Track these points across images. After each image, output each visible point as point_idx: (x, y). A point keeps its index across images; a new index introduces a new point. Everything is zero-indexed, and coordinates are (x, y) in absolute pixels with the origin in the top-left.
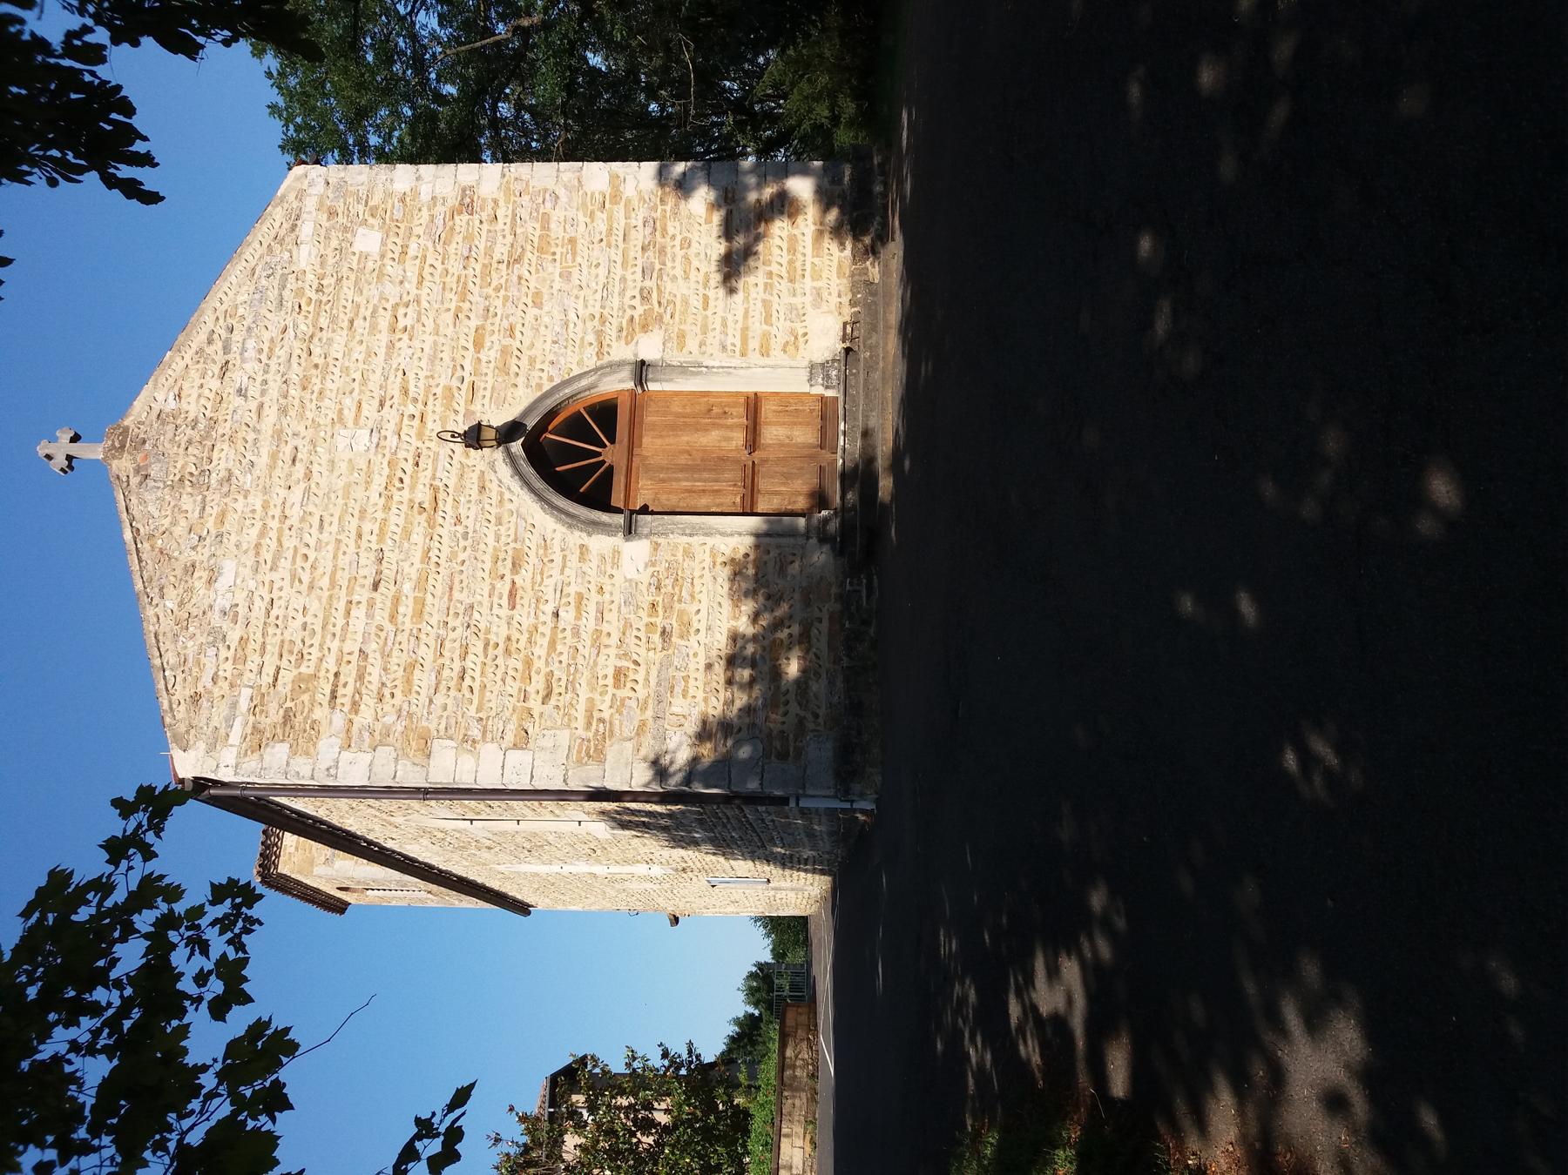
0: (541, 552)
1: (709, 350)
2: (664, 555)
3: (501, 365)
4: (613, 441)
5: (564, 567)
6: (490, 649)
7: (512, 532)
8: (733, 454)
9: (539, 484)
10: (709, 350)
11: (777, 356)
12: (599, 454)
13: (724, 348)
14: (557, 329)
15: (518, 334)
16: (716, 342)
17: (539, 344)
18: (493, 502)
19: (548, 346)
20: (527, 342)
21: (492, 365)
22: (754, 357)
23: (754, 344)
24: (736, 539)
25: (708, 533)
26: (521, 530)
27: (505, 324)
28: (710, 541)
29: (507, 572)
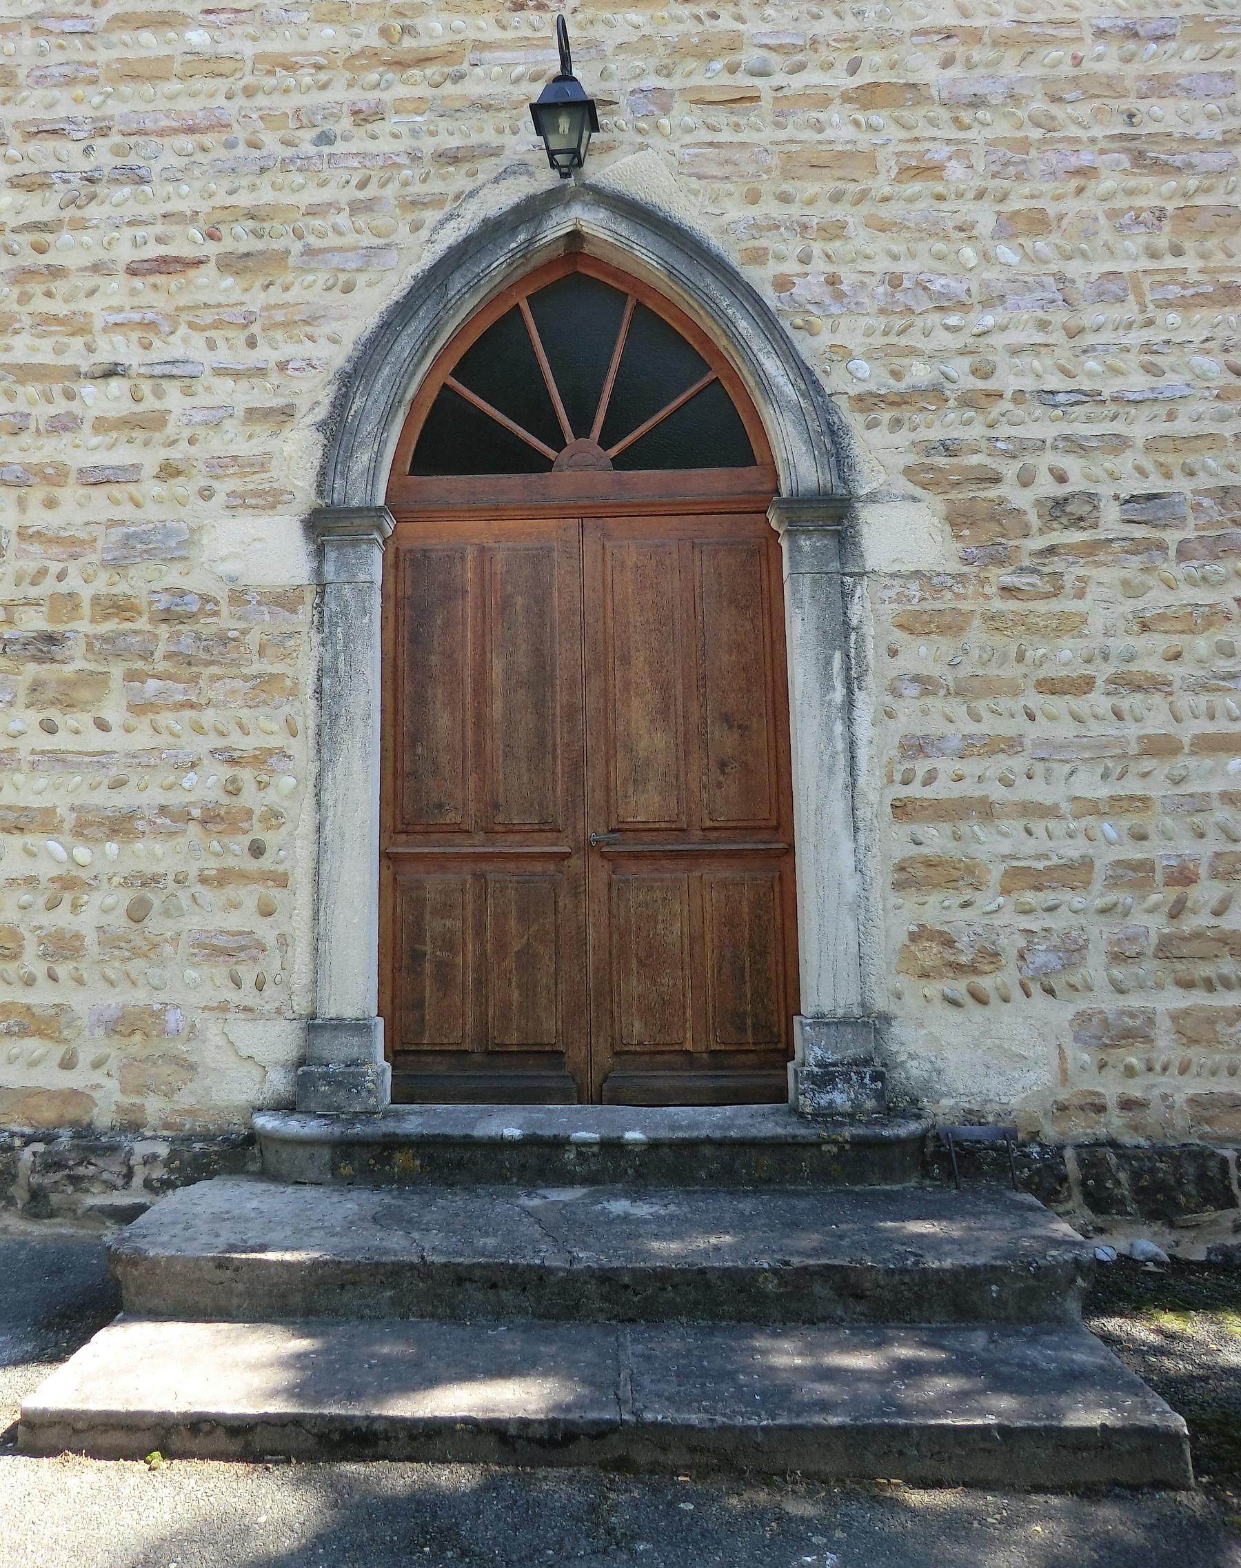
0: (279, 316)
2: (264, 624)
4: (619, 463)
6: (250, 224)
7: (333, 240)
16: (935, 726)
19: (882, 265)
23: (935, 839)
25: (325, 740)
26: (336, 260)
27: (940, 152)
28: (302, 749)
29: (227, 245)
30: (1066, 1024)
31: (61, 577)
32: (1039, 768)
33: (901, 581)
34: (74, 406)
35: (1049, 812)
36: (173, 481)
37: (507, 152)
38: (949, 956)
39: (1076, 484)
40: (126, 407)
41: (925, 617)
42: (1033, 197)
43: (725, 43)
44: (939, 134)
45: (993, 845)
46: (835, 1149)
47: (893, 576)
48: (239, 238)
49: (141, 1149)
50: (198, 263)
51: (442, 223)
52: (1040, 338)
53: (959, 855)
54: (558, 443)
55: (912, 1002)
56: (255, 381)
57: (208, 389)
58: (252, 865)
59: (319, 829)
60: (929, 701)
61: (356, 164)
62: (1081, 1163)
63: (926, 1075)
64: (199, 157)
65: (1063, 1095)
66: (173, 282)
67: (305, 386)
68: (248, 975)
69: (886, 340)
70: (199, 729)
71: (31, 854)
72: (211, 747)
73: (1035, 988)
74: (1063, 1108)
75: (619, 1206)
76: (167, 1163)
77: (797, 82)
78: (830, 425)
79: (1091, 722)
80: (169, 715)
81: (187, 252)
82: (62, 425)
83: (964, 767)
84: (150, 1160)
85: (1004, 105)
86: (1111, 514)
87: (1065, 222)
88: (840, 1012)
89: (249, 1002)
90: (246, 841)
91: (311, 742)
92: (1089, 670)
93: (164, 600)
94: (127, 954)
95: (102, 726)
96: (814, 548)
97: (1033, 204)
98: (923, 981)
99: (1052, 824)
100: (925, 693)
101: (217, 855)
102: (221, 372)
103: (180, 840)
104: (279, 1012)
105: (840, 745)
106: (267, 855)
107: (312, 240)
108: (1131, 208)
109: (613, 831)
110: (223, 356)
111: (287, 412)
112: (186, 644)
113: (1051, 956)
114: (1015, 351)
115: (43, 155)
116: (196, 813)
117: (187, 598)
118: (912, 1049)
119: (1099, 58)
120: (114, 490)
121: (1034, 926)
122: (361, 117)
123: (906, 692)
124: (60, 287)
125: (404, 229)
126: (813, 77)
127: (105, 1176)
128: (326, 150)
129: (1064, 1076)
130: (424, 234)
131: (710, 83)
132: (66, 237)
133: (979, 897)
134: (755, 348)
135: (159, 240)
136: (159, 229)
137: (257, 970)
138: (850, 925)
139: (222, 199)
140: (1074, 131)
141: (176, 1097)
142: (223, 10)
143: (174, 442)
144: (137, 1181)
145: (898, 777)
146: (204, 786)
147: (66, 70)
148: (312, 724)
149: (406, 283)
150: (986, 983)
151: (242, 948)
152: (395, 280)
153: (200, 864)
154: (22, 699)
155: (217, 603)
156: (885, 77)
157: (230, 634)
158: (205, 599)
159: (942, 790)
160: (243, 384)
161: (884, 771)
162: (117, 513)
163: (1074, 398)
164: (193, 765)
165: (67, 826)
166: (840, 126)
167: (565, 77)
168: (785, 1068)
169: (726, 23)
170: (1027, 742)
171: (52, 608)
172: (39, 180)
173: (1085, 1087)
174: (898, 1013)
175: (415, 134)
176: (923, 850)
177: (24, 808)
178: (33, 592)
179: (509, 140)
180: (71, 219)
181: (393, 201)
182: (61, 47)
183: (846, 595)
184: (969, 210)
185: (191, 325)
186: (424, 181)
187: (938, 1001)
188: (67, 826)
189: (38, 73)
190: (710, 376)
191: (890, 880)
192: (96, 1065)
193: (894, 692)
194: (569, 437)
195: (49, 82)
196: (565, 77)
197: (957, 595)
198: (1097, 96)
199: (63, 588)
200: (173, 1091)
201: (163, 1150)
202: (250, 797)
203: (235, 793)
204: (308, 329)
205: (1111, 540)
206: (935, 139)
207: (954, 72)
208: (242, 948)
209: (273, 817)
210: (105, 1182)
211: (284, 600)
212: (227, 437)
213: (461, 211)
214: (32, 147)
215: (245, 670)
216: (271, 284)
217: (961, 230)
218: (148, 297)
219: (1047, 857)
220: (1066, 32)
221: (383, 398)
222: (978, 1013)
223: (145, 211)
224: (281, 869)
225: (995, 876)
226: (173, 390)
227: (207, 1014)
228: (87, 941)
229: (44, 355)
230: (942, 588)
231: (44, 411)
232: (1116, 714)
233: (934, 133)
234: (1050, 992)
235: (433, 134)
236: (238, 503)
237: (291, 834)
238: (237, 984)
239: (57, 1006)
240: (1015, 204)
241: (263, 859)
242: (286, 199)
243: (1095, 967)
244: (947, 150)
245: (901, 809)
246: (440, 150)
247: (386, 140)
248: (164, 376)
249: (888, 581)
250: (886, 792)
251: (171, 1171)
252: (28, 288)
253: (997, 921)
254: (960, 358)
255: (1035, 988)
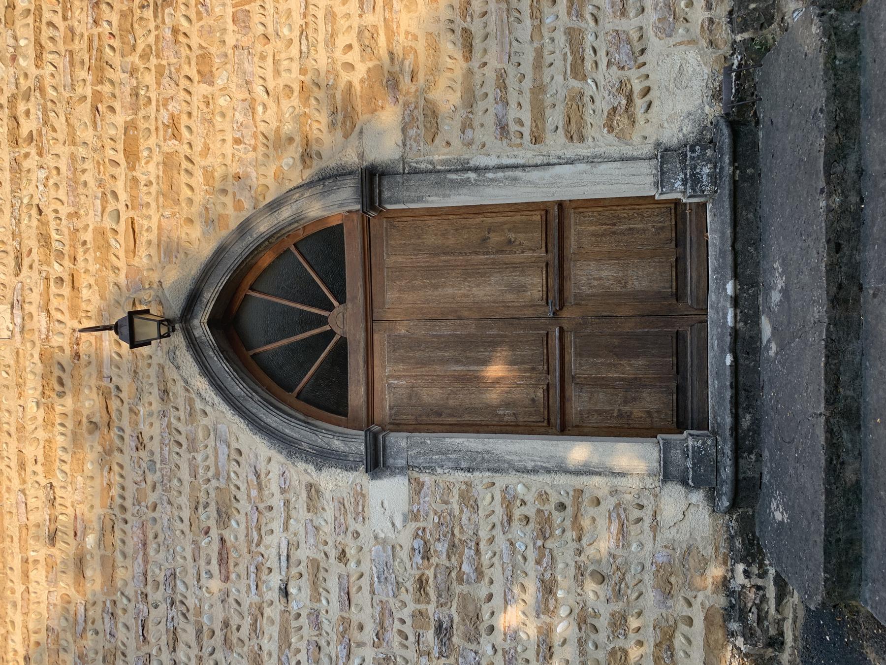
2: (429, 501)
4: (342, 300)
7: (211, 461)
16: (490, 120)
19: (228, 149)
23: (555, 117)
25: (498, 467)
26: (222, 458)
27: (165, 116)
28: (501, 480)
29: (212, 523)
30: (662, 42)
31: (403, 622)
32: (514, 59)
34: (304, 613)
35: (539, 54)
36: (348, 555)
37: (162, 362)
39: (351, 38)
40: (305, 583)
41: (428, 125)
42: (189, 63)
43: (100, 238)
44: (153, 116)
45: (559, 83)
48: (208, 518)
49: (740, 579)
50: (222, 540)
51: (203, 399)
52: (270, 60)
53: (564, 105)
54: (332, 333)
57: (295, 535)
59: (548, 471)
60: (476, 124)
61: (167, 449)
62: (742, 31)
64: (161, 538)
65: (703, 43)
66: (233, 555)
67: (295, 477)
68: (636, 513)
69: (271, 147)
70: (491, 540)
71: (564, 642)
72: (501, 533)
73: (641, 60)
74: (711, 43)
75: (776, 297)
76: (749, 565)
77: (123, 196)
78: (320, 180)
79: (488, 30)
80: (483, 558)
81: (216, 546)
82: (315, 618)
83: (513, 104)
84: (747, 574)
85: (137, 78)
86: (370, 19)
87: (204, 45)
88: (654, 172)
90: (555, 514)
91: (498, 475)
92: (459, 32)
93: (418, 559)
94: (623, 585)
95: (490, 597)
96: (389, 190)
97: (193, 62)
98: (637, 125)
99: (546, 52)
101: (564, 531)
102: (286, 528)
103: (555, 552)
104: (656, 496)
105: (500, 174)
106: (563, 501)
107: (210, 474)
108: (196, 5)
109: (547, 303)
110: (277, 526)
111: (310, 486)
112: (442, 547)
113: (622, 51)
114: (277, 73)
115: (158, 634)
116: (539, 543)
117: (416, 547)
118: (676, 130)
119: (109, 23)
120: (353, 590)
121: (605, 61)
122: (141, 444)
123: (471, 137)
124: (235, 621)
125: (205, 421)
126: (120, 186)
127: (757, 602)
128: (158, 466)
129: (693, 42)
130: (208, 409)
131: (123, 245)
132: (205, 619)
133: (588, 94)
135: (209, 563)
136: (202, 563)
139: (185, 527)
140: (151, 39)
141: (708, 558)
142: (75, 527)
143: (326, 554)
144: (760, 582)
145: (519, 141)
146: (522, 535)
147: (107, 619)
148: (487, 474)
149: (237, 419)
151: (619, 516)
152: (235, 426)
153: (570, 542)
154: (474, 646)
155: (419, 529)
156: (120, 147)
158: (416, 536)
159: (526, 116)
160: (293, 513)
162: (366, 589)
163: (304, 41)
164: (512, 544)
165: (548, 620)
166: (150, 169)
167: (116, 328)
168: (685, 204)
169: (88, 236)
170: (499, 66)
171: (421, 628)
172: (172, 635)
173: (698, 30)
176: (560, 126)
177: (538, 646)
178: (412, 638)
180: (195, 615)
181: (189, 427)
182: (93, 623)
183: (415, 172)
184: (196, 101)
185: (258, 545)
186: (177, 409)
187: (648, 116)
188: (548, 620)
189: (108, 636)
190: (293, 248)
192: (690, 604)
193: (470, 144)
195: (114, 631)
196: (116, 328)
197: (416, 108)
198: (132, 25)
199: (409, 621)
200: (705, 559)
201: (740, 567)
202: (530, 511)
203: (527, 519)
204: (263, 476)
205: (385, 19)
206: (156, 118)
207: (117, 106)
208: (619, 516)
209: (543, 497)
210: (761, 602)
211: (418, 488)
212: (323, 523)
214: (152, 639)
215: (457, 512)
216: (235, 498)
217: (208, 104)
218: (241, 569)
219: (566, 54)
220: (96, 44)
223: (192, 571)
224: (571, 493)
225: (576, 84)
226: (297, 555)
227: (658, 539)
228: (616, 609)
229: (274, 631)
230: (411, 115)
231: (308, 632)
232: (483, 16)
233: (153, 116)
234: (643, 51)
235: (150, 404)
236: (361, 515)
237: (552, 487)
239: (654, 627)
240: (193, 73)
242: (186, 489)
243: (629, 25)
244: (162, 111)
247: (153, 430)
248: (288, 560)
251: (754, 561)
252: (235, 641)
253: (602, 83)
254: (281, 105)
255: (641, 60)
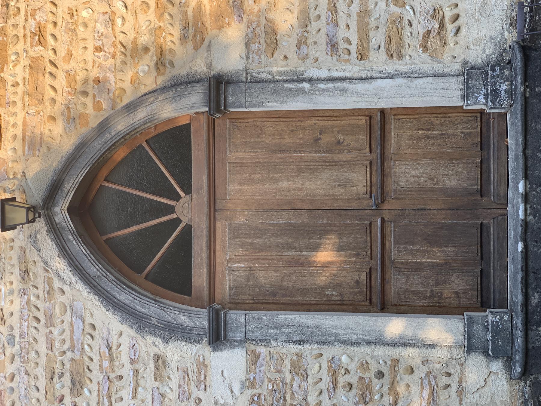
0: (106, 364)
1: (313, 52)
2: (265, 371)
3: (30, 88)
4: (188, 191)
5: (137, 386)
6: (56, 379)
7: (67, 336)
8: (355, 205)
9: (94, 269)
10: (313, 52)
11: (416, 59)
12: (170, 210)
13: (333, 46)
14: (100, 27)
15: (50, 41)
16: (322, 38)
17: (78, 53)
18: (41, 292)
19: (90, 55)
20: (62, 52)
21: (20, 89)
22: (378, 61)
23: (378, 38)
24: (385, 208)
25: (325, 340)
26: (77, 333)
27: (32, 25)
28: (328, 352)
29: (66, 392)
33: (250, 53)
37: (23, 245)
38: (434, 33)
44: (21, 25)
46: (528, 90)
47: (248, 57)
51: (61, 279)
53: (386, 27)
54: (178, 221)
55: (458, 51)
56: (140, 376)
58: (387, 378)
59: (369, 343)
60: (310, 41)
61: (26, 323)
63: (493, 45)
67: (144, 349)
68: (445, 380)
83: (342, 26)
88: (462, 87)
89: (457, 380)
90: (375, 381)
96: (233, 95)
100: (306, 44)
101: (382, 396)
104: (461, 365)
105: (330, 85)
106: (382, 370)
107: (66, 347)
109: (371, 197)
111: (157, 358)
123: (305, 52)
125: (62, 299)
128: (17, 339)
130: (66, 288)
133: (406, 18)
134: (132, 122)
137: (440, 376)
138: (419, 81)
148: (316, 346)
150: (448, 14)
152: (90, 303)
155: (254, 395)
157: (270, 388)
160: (142, 382)
161: (343, 63)
174: (462, 58)
175: (11, 292)
179: (17, 244)
186: (37, 288)
191: (397, 62)
193: (305, 58)
194: (174, 216)
197: (258, 26)
202: (353, 379)
203: (350, 386)
204: (114, 348)
206: (24, 26)
209: (364, 366)
213: (54, 268)
215: (288, 381)
217: (72, 15)
221: (152, 308)
222: (462, 21)
236: (203, 383)
238: (448, 386)
241: (385, 372)
242: (43, 361)
245: (362, 56)
246: (21, 280)
249: (250, 61)
250: (354, 62)
